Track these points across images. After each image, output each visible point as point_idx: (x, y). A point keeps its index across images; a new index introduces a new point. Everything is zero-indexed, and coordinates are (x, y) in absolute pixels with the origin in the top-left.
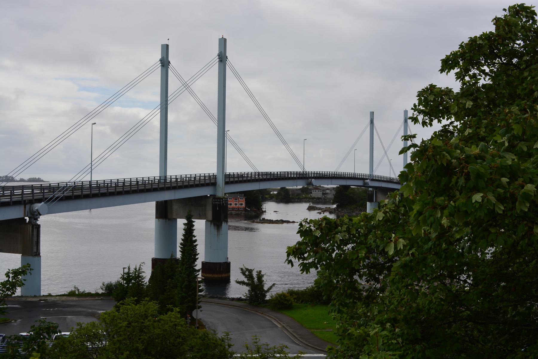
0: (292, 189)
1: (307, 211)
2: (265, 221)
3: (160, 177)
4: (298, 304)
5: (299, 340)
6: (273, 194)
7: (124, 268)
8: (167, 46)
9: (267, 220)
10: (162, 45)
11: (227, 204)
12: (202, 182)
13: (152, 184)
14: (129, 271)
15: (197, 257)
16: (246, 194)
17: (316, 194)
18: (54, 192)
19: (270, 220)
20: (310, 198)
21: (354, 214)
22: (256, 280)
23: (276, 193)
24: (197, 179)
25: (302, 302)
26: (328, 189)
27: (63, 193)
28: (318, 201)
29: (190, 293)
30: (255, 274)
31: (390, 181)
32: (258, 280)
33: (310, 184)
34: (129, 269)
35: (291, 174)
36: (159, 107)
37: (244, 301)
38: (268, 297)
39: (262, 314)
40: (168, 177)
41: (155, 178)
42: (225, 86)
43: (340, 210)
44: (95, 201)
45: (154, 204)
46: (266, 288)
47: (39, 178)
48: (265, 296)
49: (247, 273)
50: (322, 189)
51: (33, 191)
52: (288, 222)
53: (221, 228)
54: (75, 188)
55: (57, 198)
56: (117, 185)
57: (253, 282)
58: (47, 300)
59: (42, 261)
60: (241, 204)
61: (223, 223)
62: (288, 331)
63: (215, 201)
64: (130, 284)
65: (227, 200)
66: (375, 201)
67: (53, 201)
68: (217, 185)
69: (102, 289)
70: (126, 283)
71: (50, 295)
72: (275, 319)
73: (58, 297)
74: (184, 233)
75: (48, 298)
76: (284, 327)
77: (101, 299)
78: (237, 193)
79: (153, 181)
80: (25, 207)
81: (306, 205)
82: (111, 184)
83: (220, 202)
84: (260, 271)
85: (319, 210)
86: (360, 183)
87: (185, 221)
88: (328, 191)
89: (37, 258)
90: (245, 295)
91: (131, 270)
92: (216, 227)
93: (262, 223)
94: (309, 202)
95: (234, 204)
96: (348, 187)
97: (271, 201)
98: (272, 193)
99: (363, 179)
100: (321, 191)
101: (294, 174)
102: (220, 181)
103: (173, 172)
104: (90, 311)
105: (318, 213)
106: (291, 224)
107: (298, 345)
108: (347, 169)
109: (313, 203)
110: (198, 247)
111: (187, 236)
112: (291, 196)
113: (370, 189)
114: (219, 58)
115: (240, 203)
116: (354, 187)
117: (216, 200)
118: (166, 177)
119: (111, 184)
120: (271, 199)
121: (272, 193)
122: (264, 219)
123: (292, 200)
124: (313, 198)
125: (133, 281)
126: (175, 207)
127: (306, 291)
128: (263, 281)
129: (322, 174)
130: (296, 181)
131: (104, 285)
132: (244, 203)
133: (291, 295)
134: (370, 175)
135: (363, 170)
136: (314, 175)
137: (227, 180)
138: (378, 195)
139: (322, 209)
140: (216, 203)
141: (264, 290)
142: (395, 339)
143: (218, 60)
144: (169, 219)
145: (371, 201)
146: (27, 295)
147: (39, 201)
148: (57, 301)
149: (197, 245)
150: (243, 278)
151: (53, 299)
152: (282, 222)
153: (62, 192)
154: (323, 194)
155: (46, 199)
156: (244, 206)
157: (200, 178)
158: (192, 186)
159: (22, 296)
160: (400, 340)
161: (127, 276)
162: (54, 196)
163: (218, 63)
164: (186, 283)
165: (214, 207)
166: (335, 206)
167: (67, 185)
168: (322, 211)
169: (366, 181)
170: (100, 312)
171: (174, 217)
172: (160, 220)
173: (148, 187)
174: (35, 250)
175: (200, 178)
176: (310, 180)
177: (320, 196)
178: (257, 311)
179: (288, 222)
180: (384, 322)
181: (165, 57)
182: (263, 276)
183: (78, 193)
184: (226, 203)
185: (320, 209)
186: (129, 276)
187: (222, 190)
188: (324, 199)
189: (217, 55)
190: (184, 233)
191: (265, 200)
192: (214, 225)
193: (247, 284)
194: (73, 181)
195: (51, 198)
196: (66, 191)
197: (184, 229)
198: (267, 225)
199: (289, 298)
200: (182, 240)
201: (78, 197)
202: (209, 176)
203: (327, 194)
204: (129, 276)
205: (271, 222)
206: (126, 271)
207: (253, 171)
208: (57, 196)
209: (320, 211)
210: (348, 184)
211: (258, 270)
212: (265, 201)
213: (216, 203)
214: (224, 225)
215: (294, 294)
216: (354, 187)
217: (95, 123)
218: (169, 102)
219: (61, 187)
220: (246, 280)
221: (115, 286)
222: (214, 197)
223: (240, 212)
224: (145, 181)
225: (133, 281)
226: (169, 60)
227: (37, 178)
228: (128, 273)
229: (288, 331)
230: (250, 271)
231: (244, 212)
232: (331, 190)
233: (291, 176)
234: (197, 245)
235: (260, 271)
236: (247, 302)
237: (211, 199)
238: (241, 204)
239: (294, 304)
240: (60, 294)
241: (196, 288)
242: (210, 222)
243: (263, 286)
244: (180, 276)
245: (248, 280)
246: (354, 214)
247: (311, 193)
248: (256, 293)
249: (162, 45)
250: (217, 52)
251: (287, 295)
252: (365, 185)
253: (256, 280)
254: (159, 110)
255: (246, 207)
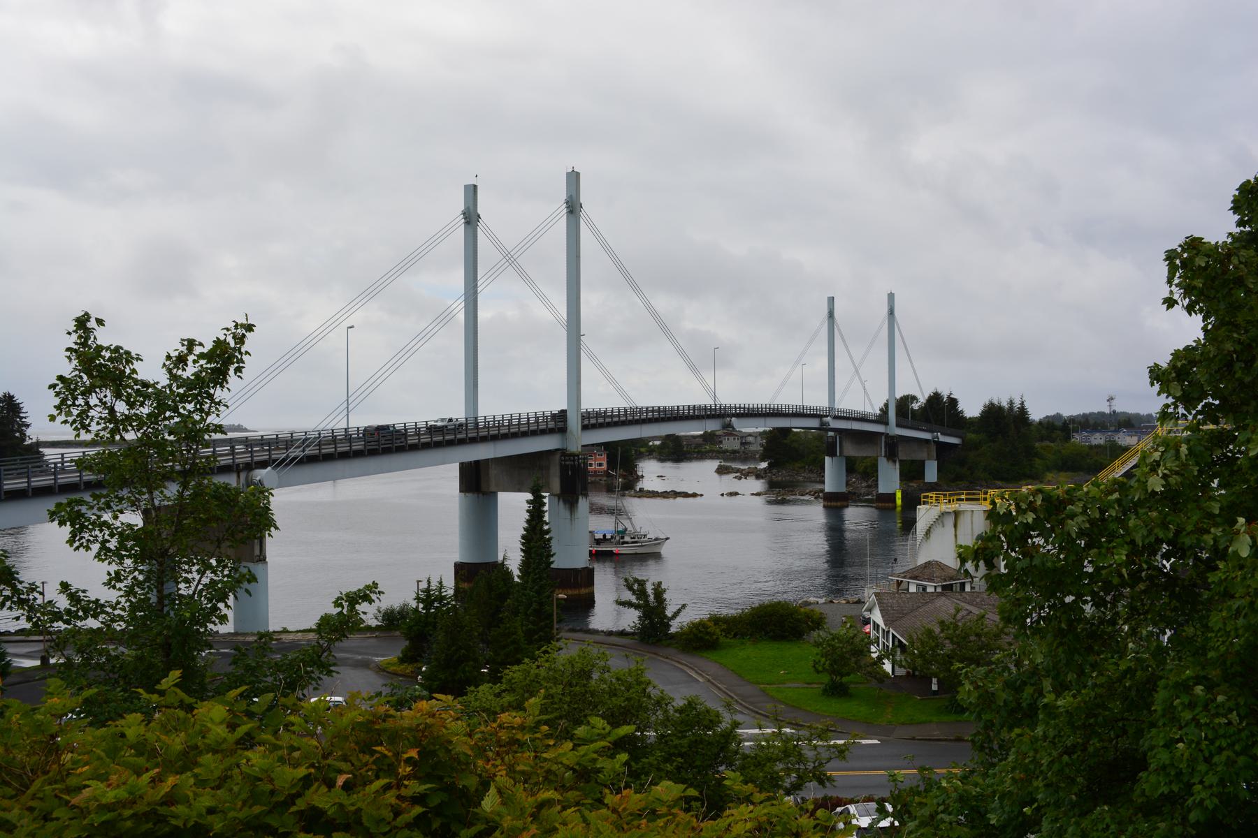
0: (686, 436)
1: (716, 475)
2: (644, 494)
3: (466, 419)
4: (728, 640)
5: (741, 704)
6: (653, 444)
7: (418, 582)
8: (475, 187)
9: (649, 492)
10: (466, 187)
11: (586, 464)
12: (533, 428)
13: (498, 427)
14: (429, 586)
15: (552, 559)
16: (607, 446)
17: (730, 444)
18: (287, 449)
19: (653, 492)
20: (718, 452)
21: (800, 478)
22: (652, 598)
23: (657, 443)
24: (515, 422)
25: (735, 635)
26: (750, 435)
27: (303, 451)
28: (733, 455)
29: (543, 624)
30: (649, 589)
31: (863, 418)
32: (655, 598)
33: (729, 425)
34: (429, 582)
35: (689, 410)
36: (463, 298)
37: (630, 637)
38: (674, 627)
39: (667, 658)
40: (481, 419)
41: (503, 417)
42: (578, 257)
43: (774, 471)
44: (340, 466)
45: (457, 465)
46: (669, 613)
47: (239, 425)
48: (669, 626)
49: (636, 587)
50: (741, 435)
51: (233, 448)
52: (685, 495)
53: (577, 507)
54: (320, 441)
55: (294, 458)
56: (605, 412)
57: (647, 601)
58: (280, 639)
59: (269, 571)
60: (600, 465)
61: (580, 497)
62: (720, 689)
63: (565, 461)
64: (430, 609)
65: (587, 459)
66: (840, 455)
67: (287, 465)
68: (568, 430)
69: (376, 618)
70: (423, 609)
71: (285, 631)
72: (691, 668)
73: (300, 634)
74: (528, 518)
75: (283, 636)
76: (709, 681)
77: (376, 637)
78: (593, 445)
79: (59, 465)
80: (239, 477)
81: (714, 464)
82: (63, 464)
83: (574, 461)
84: (660, 583)
85: (736, 473)
86: (815, 423)
87: (530, 496)
88: (750, 439)
89: (260, 566)
90: (633, 625)
91: (432, 584)
92: (567, 506)
93: (639, 497)
94: (718, 458)
95: (598, 463)
96: (786, 431)
97: (649, 459)
98: (651, 443)
99: (820, 416)
100: (738, 439)
101: (589, 418)
102: (574, 423)
103: (492, 408)
104: (360, 657)
105: (736, 477)
106: (691, 500)
107: (742, 713)
108: (789, 398)
109: (725, 460)
110: (553, 543)
111: (534, 523)
112: (685, 449)
113: (831, 434)
114: (567, 208)
115: (598, 463)
116: (798, 430)
117: (567, 458)
118: (476, 418)
119: (63, 464)
120: (649, 455)
121: (651, 443)
122: (641, 490)
123: (688, 456)
124: (726, 452)
125: (436, 604)
126: (494, 472)
127: (740, 617)
128: (665, 600)
129: (744, 408)
130: (704, 421)
131: (379, 612)
132: (604, 463)
133: (715, 624)
134: (831, 409)
135: (817, 399)
136: (694, 412)
137: (586, 422)
138: (844, 444)
139: (743, 470)
140: (567, 463)
141: (666, 616)
142: (1225, 716)
143: (565, 211)
144: (484, 493)
145: (832, 454)
146: (246, 632)
147: (263, 465)
148: (299, 640)
149: (550, 539)
150: (628, 596)
151: (291, 637)
152: (676, 494)
153: (301, 449)
154: (742, 444)
155: (275, 461)
156: (605, 467)
157: (519, 422)
158: (525, 434)
159: (236, 634)
160: (1234, 716)
161: (425, 596)
162: (288, 455)
163: (565, 217)
164: (535, 606)
165: (564, 469)
166: (764, 465)
167: (319, 434)
168: (744, 475)
169: (825, 419)
170: (377, 659)
171: (493, 489)
172: (467, 494)
173: (494, 432)
174: (257, 552)
175: (519, 422)
176: (728, 419)
177: (736, 448)
178: (655, 654)
179: (685, 495)
180: (1191, 684)
181: (471, 208)
182: (664, 591)
183: (328, 450)
184: (584, 463)
185: (738, 471)
186: (429, 596)
187: (579, 440)
188: (744, 452)
189: (563, 201)
190: (528, 518)
191: (641, 456)
192: (565, 502)
193: (637, 607)
194: (329, 427)
195: (284, 460)
196: (309, 446)
197: (528, 511)
198: (646, 501)
199: (712, 629)
200: (525, 529)
201: (328, 458)
202: (626, 410)
203: (750, 443)
204: (429, 596)
205: (654, 494)
206: (424, 585)
207: (627, 406)
208: (293, 455)
209: (738, 474)
210: (788, 426)
211: (656, 581)
212: (641, 458)
213: (567, 463)
214: (583, 504)
215: (720, 623)
216: (798, 430)
217: (352, 327)
218: (479, 289)
219: (309, 438)
220: (633, 599)
221: (399, 613)
222: (562, 452)
223: (598, 479)
224: (419, 428)
225: (436, 604)
226: (479, 212)
227: (236, 425)
228: (428, 591)
229: (720, 689)
230: (642, 583)
231: (605, 478)
232: (756, 437)
233: (694, 412)
234: (550, 539)
235: (660, 583)
236: (636, 637)
237: (558, 457)
238: (600, 465)
239: (722, 639)
240: (302, 629)
241: (553, 615)
242: (556, 498)
243: (664, 609)
244: (523, 594)
245: (637, 599)
246: (800, 478)
247: (721, 442)
248: (651, 622)
249: (466, 187)
250: (564, 196)
251: (709, 624)
252: (824, 428)
253: (652, 598)
254: (463, 304)
255: (608, 469)
